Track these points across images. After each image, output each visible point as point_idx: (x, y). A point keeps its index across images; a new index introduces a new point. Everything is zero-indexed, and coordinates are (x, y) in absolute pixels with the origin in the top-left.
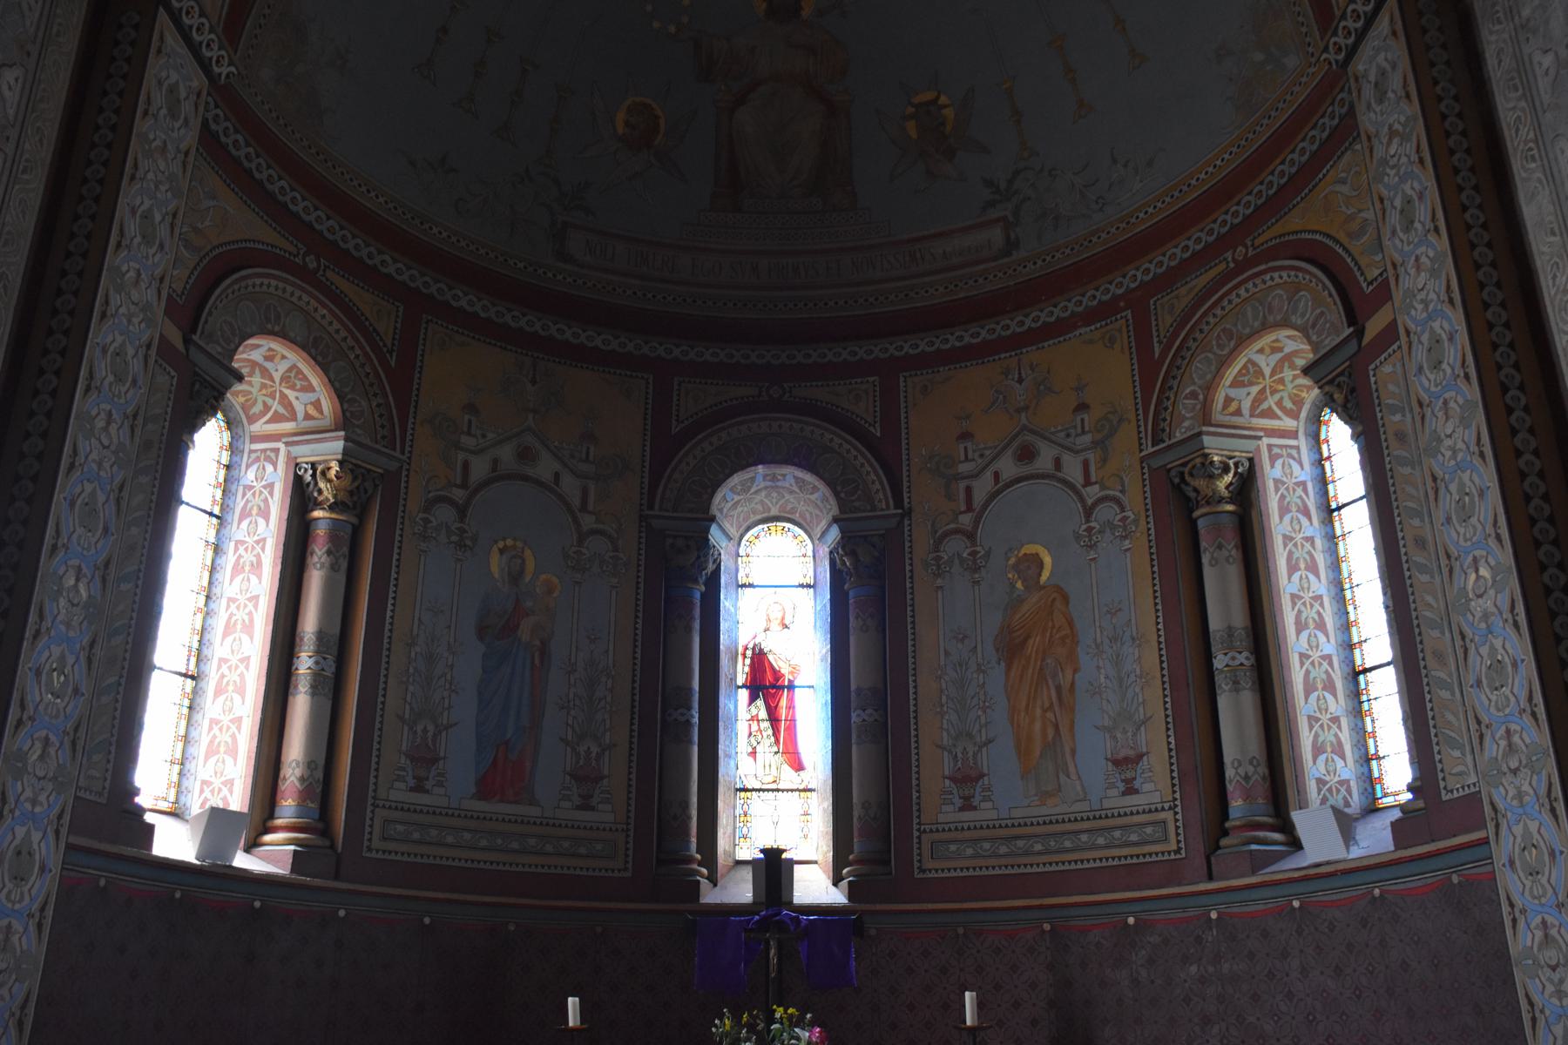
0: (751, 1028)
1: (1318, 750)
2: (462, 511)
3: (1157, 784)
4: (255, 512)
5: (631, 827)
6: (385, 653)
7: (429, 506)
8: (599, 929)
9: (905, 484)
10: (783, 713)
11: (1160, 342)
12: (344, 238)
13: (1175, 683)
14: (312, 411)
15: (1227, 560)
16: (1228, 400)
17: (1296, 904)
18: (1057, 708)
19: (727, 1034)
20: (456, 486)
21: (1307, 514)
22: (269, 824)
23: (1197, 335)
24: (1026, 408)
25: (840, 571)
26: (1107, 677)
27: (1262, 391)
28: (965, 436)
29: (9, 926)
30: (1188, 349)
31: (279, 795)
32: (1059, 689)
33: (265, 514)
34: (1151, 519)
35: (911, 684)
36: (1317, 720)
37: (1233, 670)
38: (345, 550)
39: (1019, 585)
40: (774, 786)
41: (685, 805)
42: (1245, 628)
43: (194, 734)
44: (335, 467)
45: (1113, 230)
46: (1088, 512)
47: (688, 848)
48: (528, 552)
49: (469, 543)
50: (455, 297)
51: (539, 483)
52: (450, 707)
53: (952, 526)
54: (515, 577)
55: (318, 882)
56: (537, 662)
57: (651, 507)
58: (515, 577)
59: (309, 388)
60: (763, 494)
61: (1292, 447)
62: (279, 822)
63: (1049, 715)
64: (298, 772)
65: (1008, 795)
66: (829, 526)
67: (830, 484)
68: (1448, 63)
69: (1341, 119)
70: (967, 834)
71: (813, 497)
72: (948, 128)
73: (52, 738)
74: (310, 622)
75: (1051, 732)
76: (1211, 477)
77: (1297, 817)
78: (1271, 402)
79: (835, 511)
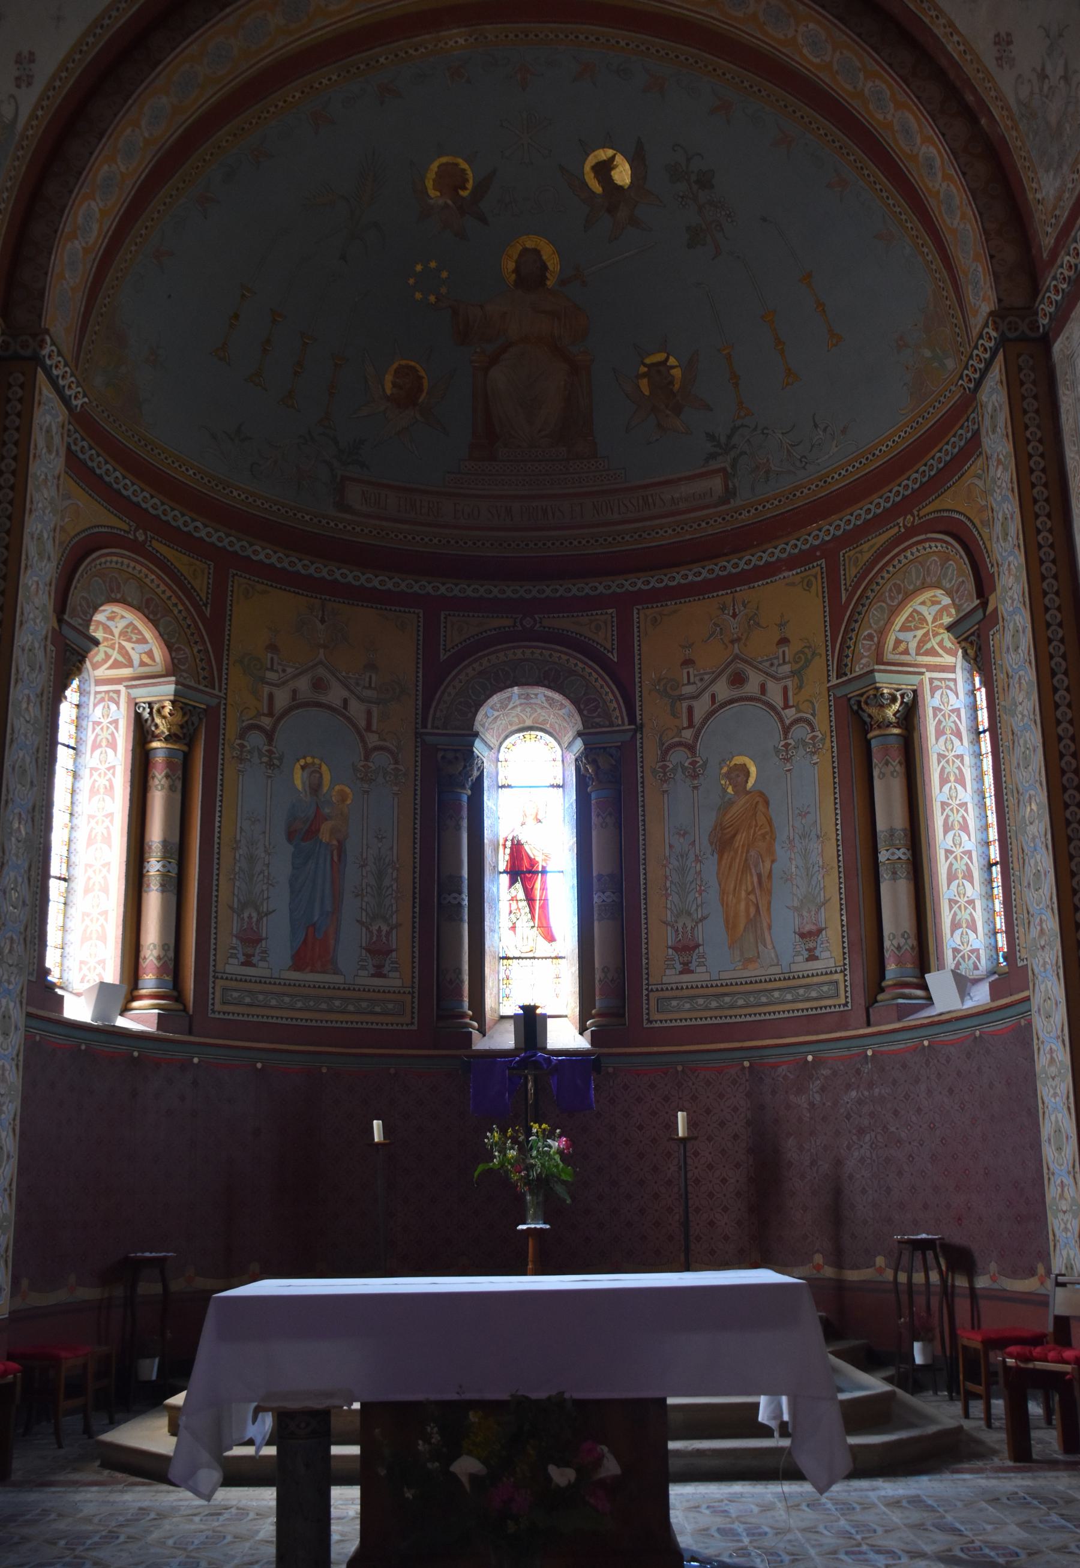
0: (515, 1141)
1: (955, 926)
2: (270, 736)
3: (832, 953)
4: (104, 743)
5: (416, 990)
6: (216, 856)
7: (243, 734)
8: (392, 1071)
9: (638, 704)
10: (537, 894)
11: (846, 590)
12: (165, 513)
13: (848, 873)
14: (146, 660)
15: (892, 774)
16: (898, 642)
17: (926, 1043)
18: (758, 891)
19: (496, 1144)
20: (264, 715)
21: (959, 736)
22: (136, 993)
23: (891, 569)
24: (739, 640)
25: (584, 776)
26: (797, 867)
27: (926, 634)
28: (688, 662)
29: (3, 1066)
30: (867, 598)
31: (141, 971)
32: (759, 876)
33: (113, 745)
34: (834, 739)
35: (642, 871)
36: (956, 902)
37: (893, 863)
38: (179, 773)
39: (730, 790)
40: (531, 955)
41: (459, 971)
42: (904, 830)
44: (168, 707)
45: (813, 487)
46: (786, 730)
47: (462, 1007)
48: (324, 768)
49: (276, 762)
50: (255, 552)
51: (329, 707)
52: (268, 898)
53: (677, 739)
54: (315, 789)
55: (177, 1037)
56: (336, 859)
57: (425, 726)
58: (315, 789)
59: (144, 641)
60: (519, 709)
61: (949, 680)
62: (143, 992)
63: (752, 897)
64: (155, 953)
65: (718, 961)
66: (574, 739)
67: (575, 702)
68: (1037, 411)
69: (966, 443)
70: (685, 992)
71: (561, 712)
72: (677, 386)
73: (15, 937)
74: (156, 833)
75: (752, 910)
76: (882, 706)
78: (934, 643)
79: (580, 727)
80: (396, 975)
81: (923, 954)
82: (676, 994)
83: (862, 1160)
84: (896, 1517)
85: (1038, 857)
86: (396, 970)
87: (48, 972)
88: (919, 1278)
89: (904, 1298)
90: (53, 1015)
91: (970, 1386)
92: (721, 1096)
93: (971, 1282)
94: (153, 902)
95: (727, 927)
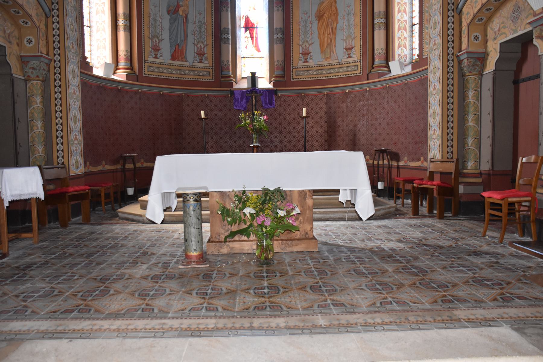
1: (399, 46)
3: (356, 56)
13: (364, 27)
32: (332, 29)
41: (228, 61)
43: (92, 43)
63: (329, 36)
64: (124, 53)
65: (317, 58)
70: (305, 69)
74: (121, 10)
75: (329, 41)
77: (391, 63)
80: (207, 62)
81: (388, 56)
82: (301, 69)
83: (363, 125)
84: (380, 230)
85: (436, 17)
86: (207, 60)
87: (86, 58)
88: (381, 162)
89: (376, 169)
90: (90, 73)
91: (398, 195)
92: (317, 104)
93: (398, 163)
94: (122, 35)
95: (320, 47)
